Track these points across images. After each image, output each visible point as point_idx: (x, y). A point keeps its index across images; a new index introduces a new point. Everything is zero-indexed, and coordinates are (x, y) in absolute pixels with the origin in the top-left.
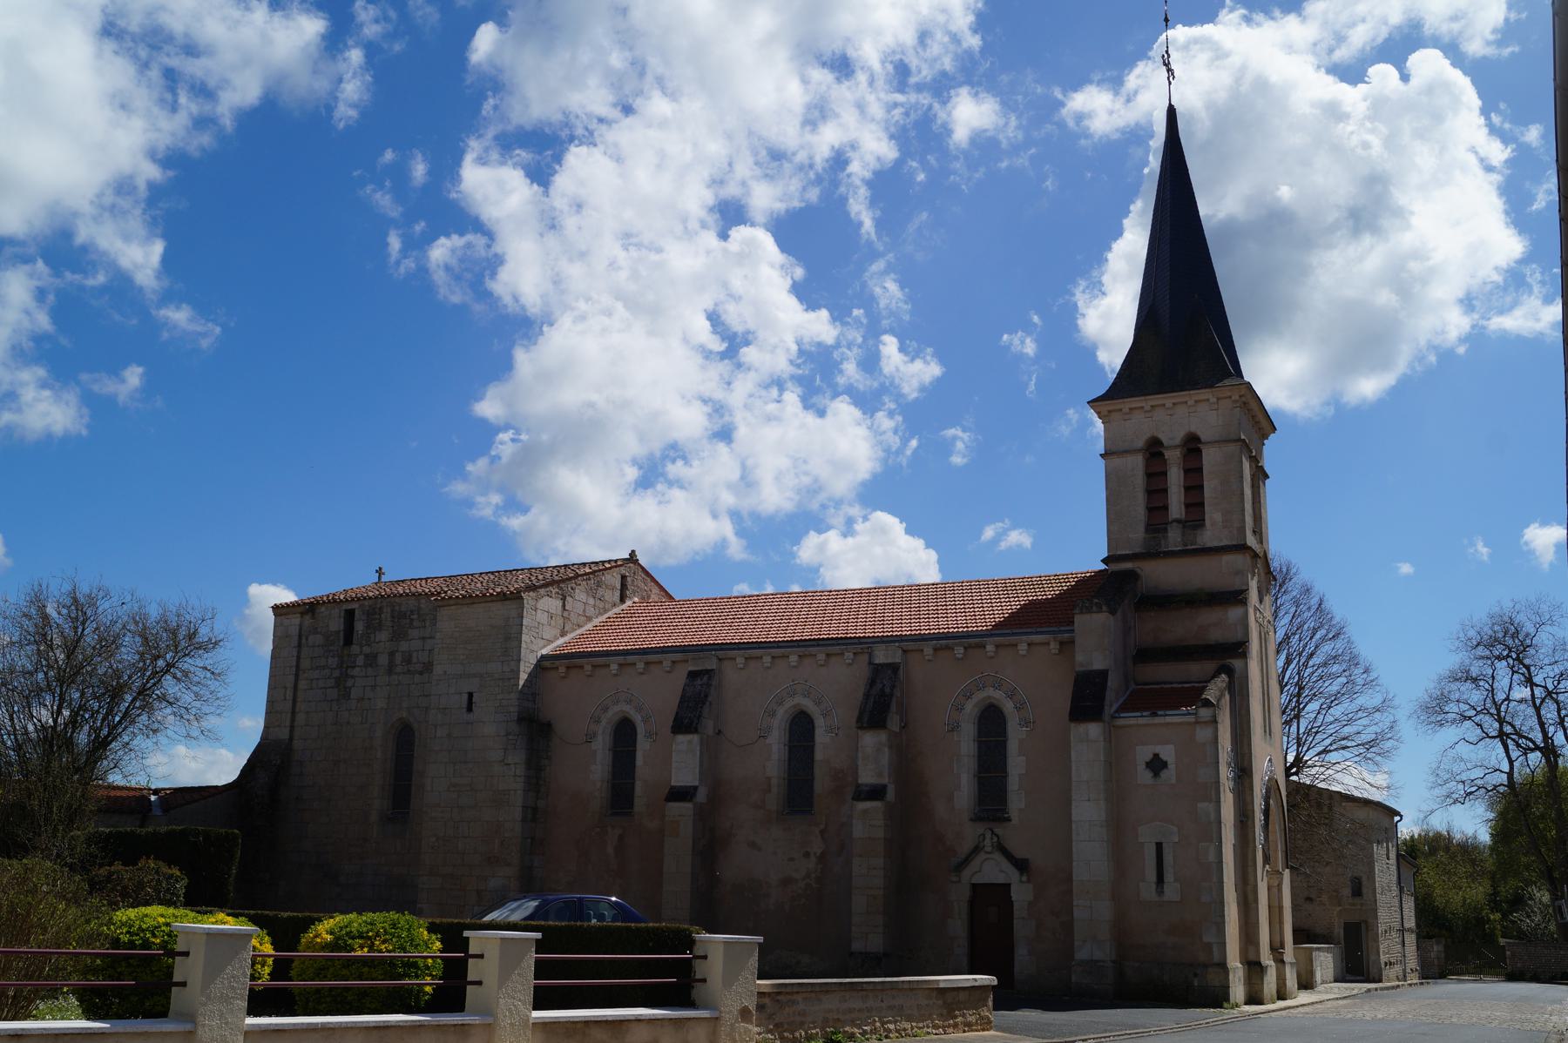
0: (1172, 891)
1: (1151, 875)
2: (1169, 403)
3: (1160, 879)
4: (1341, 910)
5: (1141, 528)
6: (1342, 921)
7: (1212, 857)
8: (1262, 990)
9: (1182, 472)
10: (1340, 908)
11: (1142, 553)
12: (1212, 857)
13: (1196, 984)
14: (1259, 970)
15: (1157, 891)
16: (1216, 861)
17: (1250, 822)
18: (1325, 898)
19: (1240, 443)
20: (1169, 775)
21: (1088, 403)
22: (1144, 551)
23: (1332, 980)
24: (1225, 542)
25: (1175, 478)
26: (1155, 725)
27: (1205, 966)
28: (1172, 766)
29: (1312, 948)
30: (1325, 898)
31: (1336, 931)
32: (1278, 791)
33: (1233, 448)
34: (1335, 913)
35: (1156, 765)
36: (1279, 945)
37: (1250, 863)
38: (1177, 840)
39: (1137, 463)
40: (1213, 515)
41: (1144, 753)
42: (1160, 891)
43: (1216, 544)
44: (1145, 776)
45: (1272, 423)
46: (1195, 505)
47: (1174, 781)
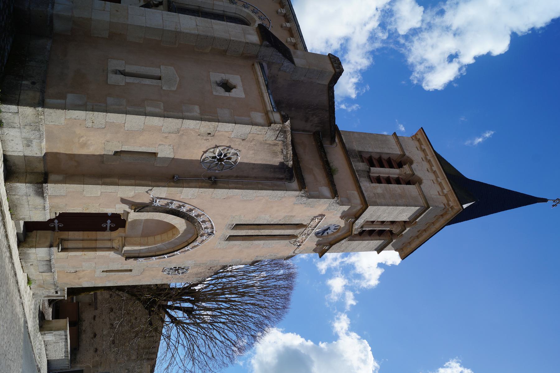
0: (114, 79)
1: (129, 69)
2: (435, 168)
3: (124, 73)
4: (90, 367)
5: (360, 149)
6: (84, 369)
7: (149, 109)
8: (19, 182)
9: (397, 176)
10: (91, 367)
11: (346, 148)
12: (149, 109)
13: (24, 82)
14: (40, 181)
15: (116, 70)
16: (146, 112)
17: (172, 184)
18: (97, 359)
19: (426, 206)
20: (221, 92)
21: (422, 128)
22: (347, 149)
23: (49, 359)
24: (366, 194)
25: (394, 172)
26: (260, 88)
27: (43, 92)
28: (227, 94)
29: (66, 329)
30: (97, 359)
31: (78, 365)
32: (186, 244)
33: (422, 202)
34: (89, 364)
35: (227, 87)
36: (65, 246)
37: (138, 182)
38: (164, 88)
39: (395, 150)
40: (380, 188)
41: (234, 79)
42: (116, 72)
43: (363, 188)
44: (218, 77)
45: (415, 250)
46: (379, 180)
47: (214, 93)
